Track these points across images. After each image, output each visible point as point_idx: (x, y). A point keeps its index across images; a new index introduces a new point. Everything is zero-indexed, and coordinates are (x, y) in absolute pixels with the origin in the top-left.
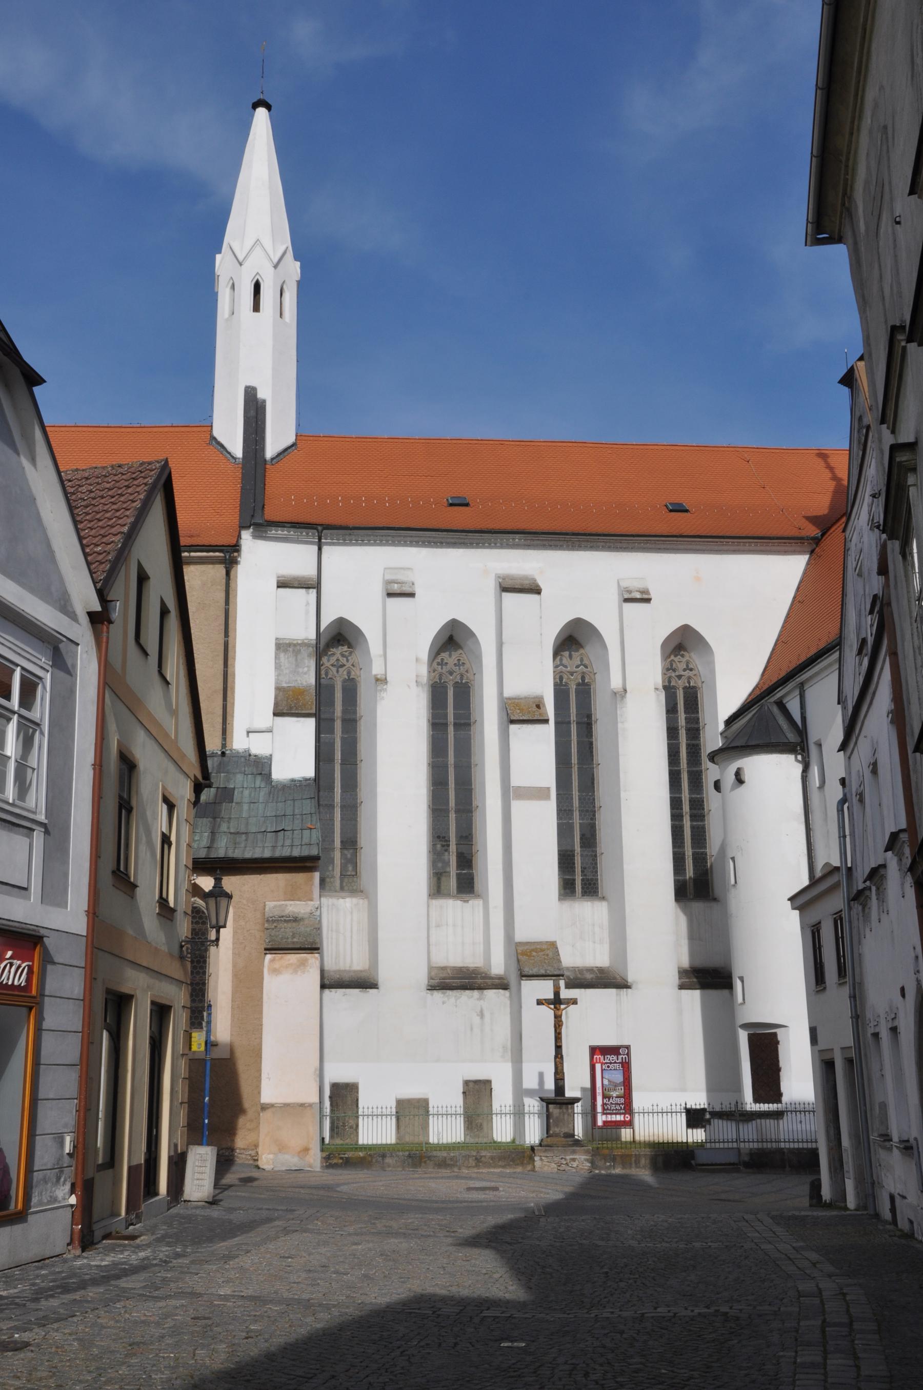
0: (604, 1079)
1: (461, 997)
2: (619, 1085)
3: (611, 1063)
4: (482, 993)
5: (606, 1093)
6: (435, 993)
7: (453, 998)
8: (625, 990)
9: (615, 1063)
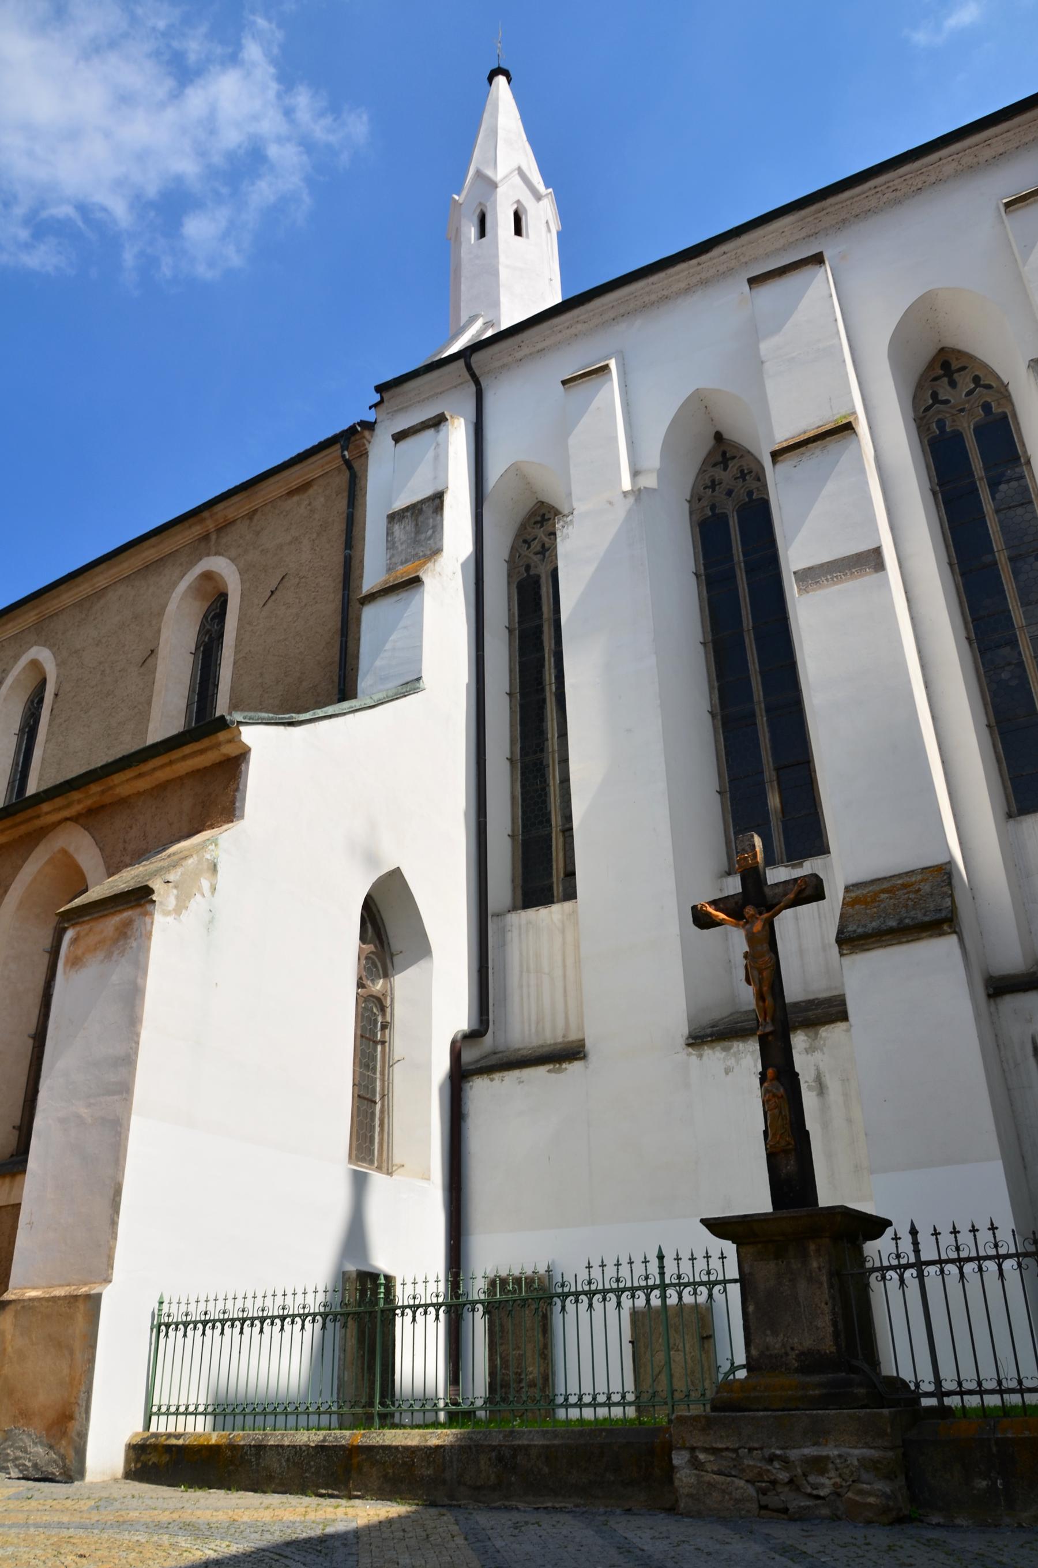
4: (817, 1034)
6: (707, 1052)
7: (749, 1056)
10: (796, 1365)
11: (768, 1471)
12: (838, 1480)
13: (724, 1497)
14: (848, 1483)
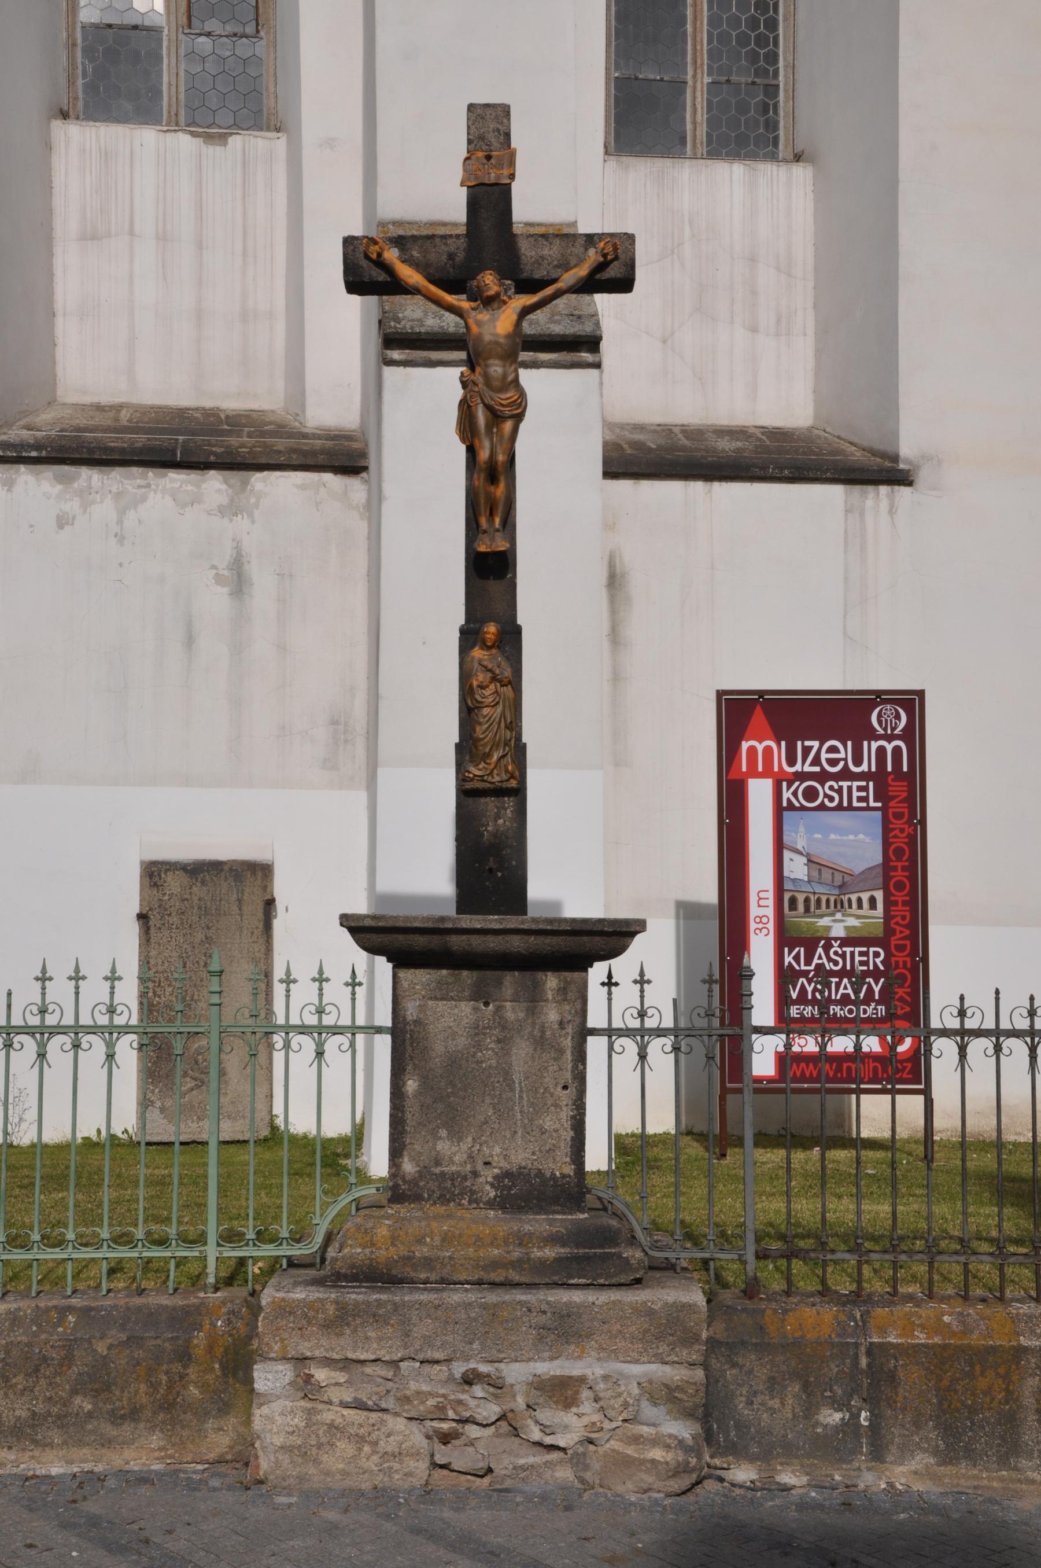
0: (787, 855)
1: (144, 499)
2: (862, 880)
3: (823, 777)
4: (245, 483)
5: (797, 918)
7: (109, 502)
8: (883, 489)
9: (846, 774)
10: (492, 1194)
11: (460, 1402)
12: (596, 1418)
13: (360, 1449)
14: (614, 1425)
